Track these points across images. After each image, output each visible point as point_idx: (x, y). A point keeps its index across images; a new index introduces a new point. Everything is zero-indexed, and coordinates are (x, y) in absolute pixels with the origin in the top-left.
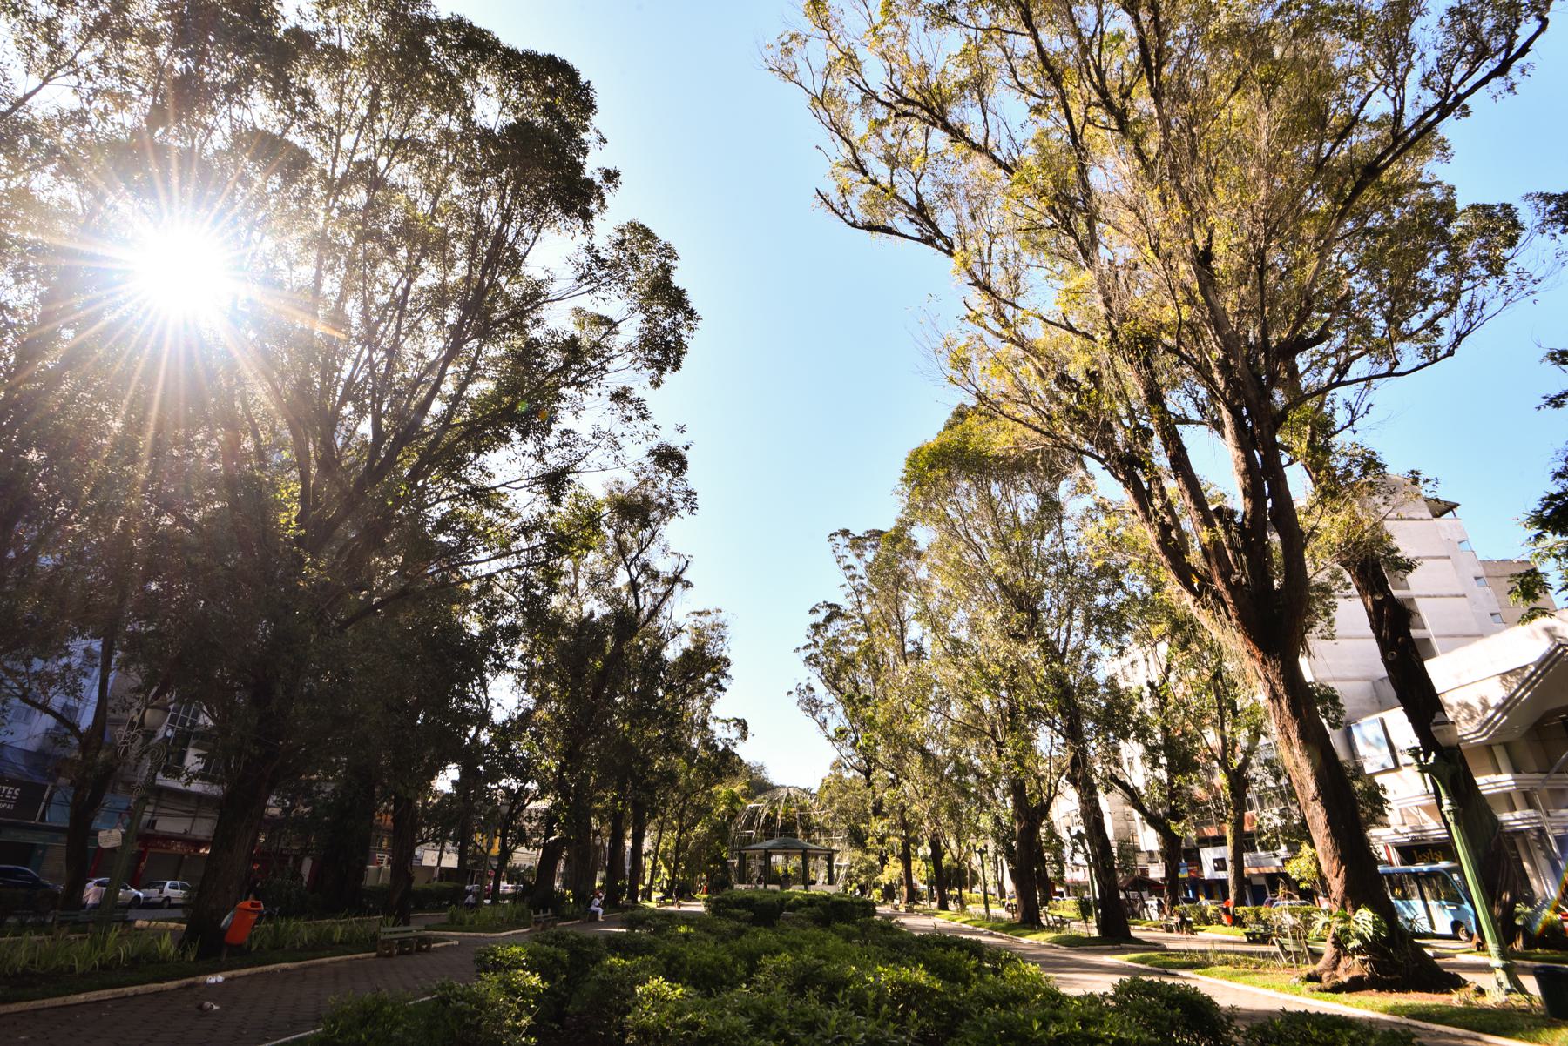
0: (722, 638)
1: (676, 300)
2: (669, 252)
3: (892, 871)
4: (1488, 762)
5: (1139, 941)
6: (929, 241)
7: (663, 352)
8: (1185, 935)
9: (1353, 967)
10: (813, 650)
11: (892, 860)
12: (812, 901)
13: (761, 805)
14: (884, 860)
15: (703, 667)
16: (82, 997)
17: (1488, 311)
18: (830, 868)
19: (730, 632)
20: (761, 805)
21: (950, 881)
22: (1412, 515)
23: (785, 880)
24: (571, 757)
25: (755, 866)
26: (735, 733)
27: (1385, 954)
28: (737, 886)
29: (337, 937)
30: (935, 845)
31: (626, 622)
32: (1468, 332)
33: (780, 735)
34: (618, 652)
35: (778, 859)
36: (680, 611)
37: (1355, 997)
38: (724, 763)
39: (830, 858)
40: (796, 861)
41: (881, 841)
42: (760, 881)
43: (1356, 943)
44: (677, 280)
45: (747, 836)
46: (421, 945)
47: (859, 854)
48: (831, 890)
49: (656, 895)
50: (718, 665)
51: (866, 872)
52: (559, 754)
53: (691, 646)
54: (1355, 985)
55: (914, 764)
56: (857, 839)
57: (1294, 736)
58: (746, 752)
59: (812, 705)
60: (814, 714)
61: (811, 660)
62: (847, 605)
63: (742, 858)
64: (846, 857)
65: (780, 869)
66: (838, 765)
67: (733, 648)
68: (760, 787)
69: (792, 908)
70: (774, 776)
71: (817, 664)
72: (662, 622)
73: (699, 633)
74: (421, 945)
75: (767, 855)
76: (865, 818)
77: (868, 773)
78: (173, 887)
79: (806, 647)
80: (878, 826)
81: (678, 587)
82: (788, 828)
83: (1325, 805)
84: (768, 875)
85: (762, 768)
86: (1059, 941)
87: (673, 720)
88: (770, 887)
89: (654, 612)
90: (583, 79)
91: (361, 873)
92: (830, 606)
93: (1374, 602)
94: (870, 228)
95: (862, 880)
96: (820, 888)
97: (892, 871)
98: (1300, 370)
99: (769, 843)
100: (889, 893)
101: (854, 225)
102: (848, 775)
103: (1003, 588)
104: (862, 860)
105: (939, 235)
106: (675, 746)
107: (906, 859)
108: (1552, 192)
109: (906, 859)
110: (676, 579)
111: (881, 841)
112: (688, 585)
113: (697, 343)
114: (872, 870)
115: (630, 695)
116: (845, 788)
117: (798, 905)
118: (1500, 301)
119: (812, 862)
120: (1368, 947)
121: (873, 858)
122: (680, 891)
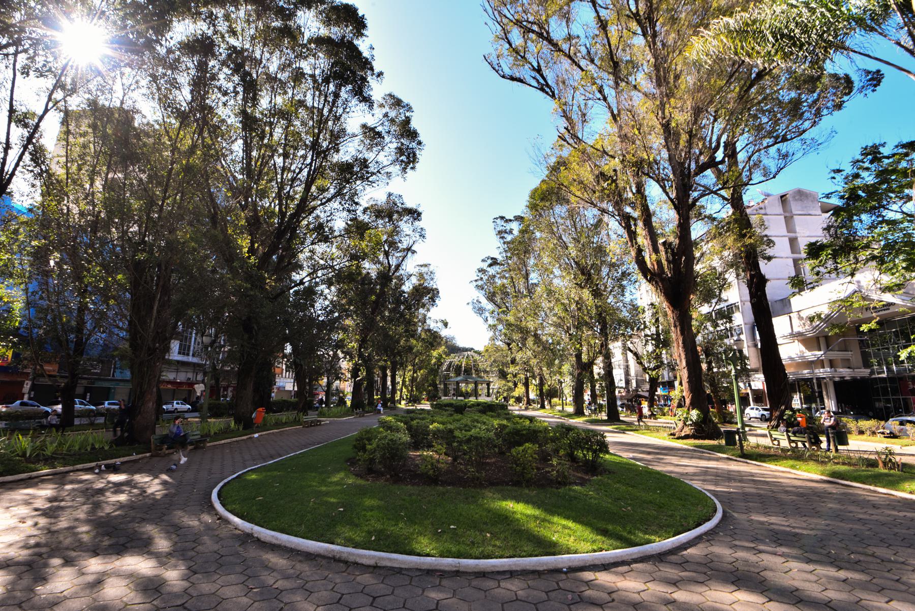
0: (432, 279)
1: (413, 135)
2: (410, 109)
3: (520, 391)
4: (816, 345)
5: (623, 421)
6: (542, 90)
7: (408, 158)
8: (652, 420)
9: (687, 431)
10: (480, 283)
11: (520, 385)
12: (479, 404)
13: (455, 359)
14: (515, 385)
15: (425, 294)
16: (223, 442)
17: (795, 157)
18: (488, 389)
19: (437, 277)
20: (455, 359)
21: (549, 394)
22: (811, 212)
23: (467, 395)
24: (363, 343)
25: (452, 387)
26: (440, 325)
27: (701, 426)
28: (443, 398)
29: (284, 421)
30: (541, 380)
31: (385, 276)
32: (784, 167)
33: (462, 321)
34: (382, 293)
35: (463, 385)
36: (410, 266)
37: (685, 441)
38: (434, 339)
39: (488, 385)
40: (471, 386)
41: (515, 376)
42: (454, 395)
43: (690, 422)
44: (414, 124)
45: (445, 374)
46: (316, 424)
47: (504, 382)
48: (488, 399)
49: (403, 402)
50: (433, 294)
51: (508, 390)
52: (357, 341)
53: (417, 283)
54: (686, 437)
55: (530, 342)
56: (503, 375)
57: (681, 343)
58: (444, 333)
59: (480, 311)
60: (481, 314)
61: (480, 288)
62: (500, 258)
63: (445, 385)
64: (497, 384)
65: (463, 389)
66: (493, 339)
67: (438, 283)
68: (454, 349)
69: (469, 407)
70: (461, 343)
71: (483, 289)
72: (401, 272)
73: (421, 276)
74: (316, 424)
75: (458, 383)
76: (506, 364)
77: (509, 345)
78: (178, 403)
79: (476, 281)
80: (512, 369)
81: (410, 254)
82: (468, 371)
83: (688, 370)
84: (458, 392)
85: (453, 338)
86: (587, 421)
87: (409, 323)
88: (459, 398)
89: (398, 267)
90: (360, 13)
91: (270, 396)
92: (492, 258)
93: (751, 275)
94: (512, 79)
95: (505, 395)
96: (483, 399)
97: (520, 391)
98: (738, 150)
99: (459, 378)
100: (518, 400)
101: (503, 77)
102: (499, 343)
103: (576, 263)
104: (505, 385)
105: (548, 85)
106: (413, 334)
107: (526, 385)
108: (870, 69)
109: (526, 385)
110: (409, 249)
111: (515, 376)
112: (414, 252)
113: (422, 155)
114: (510, 390)
115: (388, 309)
116: (497, 349)
117: (473, 405)
118: (802, 152)
119: (480, 387)
120: (695, 424)
121: (511, 384)
122: (414, 400)
